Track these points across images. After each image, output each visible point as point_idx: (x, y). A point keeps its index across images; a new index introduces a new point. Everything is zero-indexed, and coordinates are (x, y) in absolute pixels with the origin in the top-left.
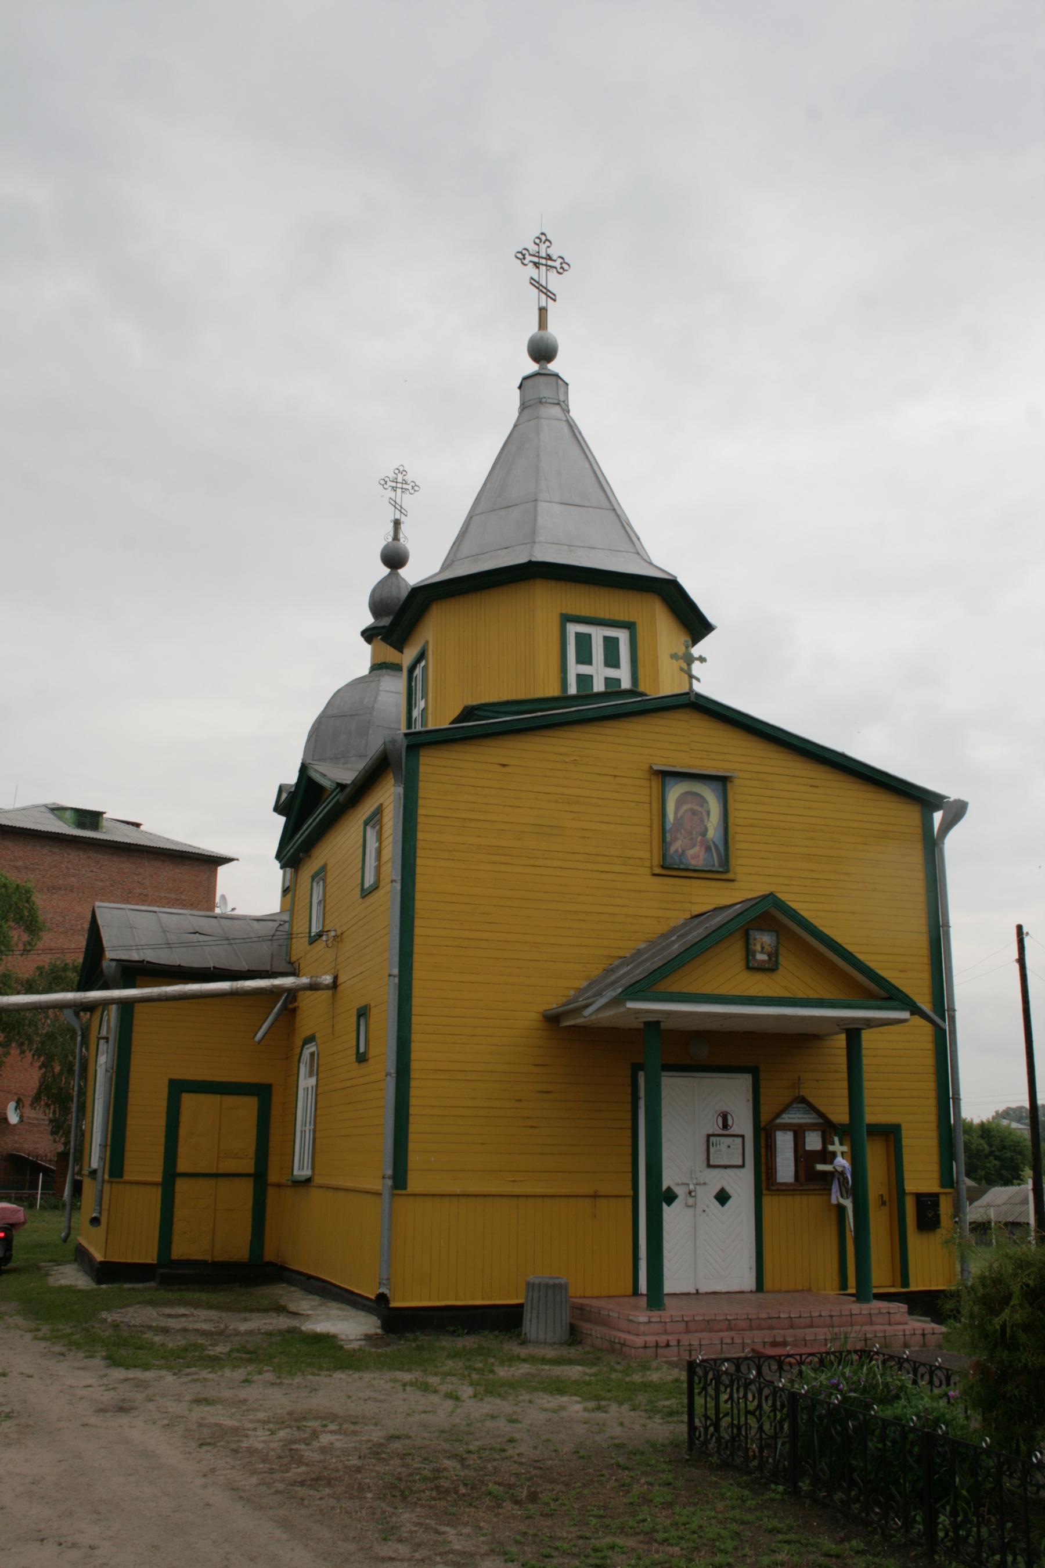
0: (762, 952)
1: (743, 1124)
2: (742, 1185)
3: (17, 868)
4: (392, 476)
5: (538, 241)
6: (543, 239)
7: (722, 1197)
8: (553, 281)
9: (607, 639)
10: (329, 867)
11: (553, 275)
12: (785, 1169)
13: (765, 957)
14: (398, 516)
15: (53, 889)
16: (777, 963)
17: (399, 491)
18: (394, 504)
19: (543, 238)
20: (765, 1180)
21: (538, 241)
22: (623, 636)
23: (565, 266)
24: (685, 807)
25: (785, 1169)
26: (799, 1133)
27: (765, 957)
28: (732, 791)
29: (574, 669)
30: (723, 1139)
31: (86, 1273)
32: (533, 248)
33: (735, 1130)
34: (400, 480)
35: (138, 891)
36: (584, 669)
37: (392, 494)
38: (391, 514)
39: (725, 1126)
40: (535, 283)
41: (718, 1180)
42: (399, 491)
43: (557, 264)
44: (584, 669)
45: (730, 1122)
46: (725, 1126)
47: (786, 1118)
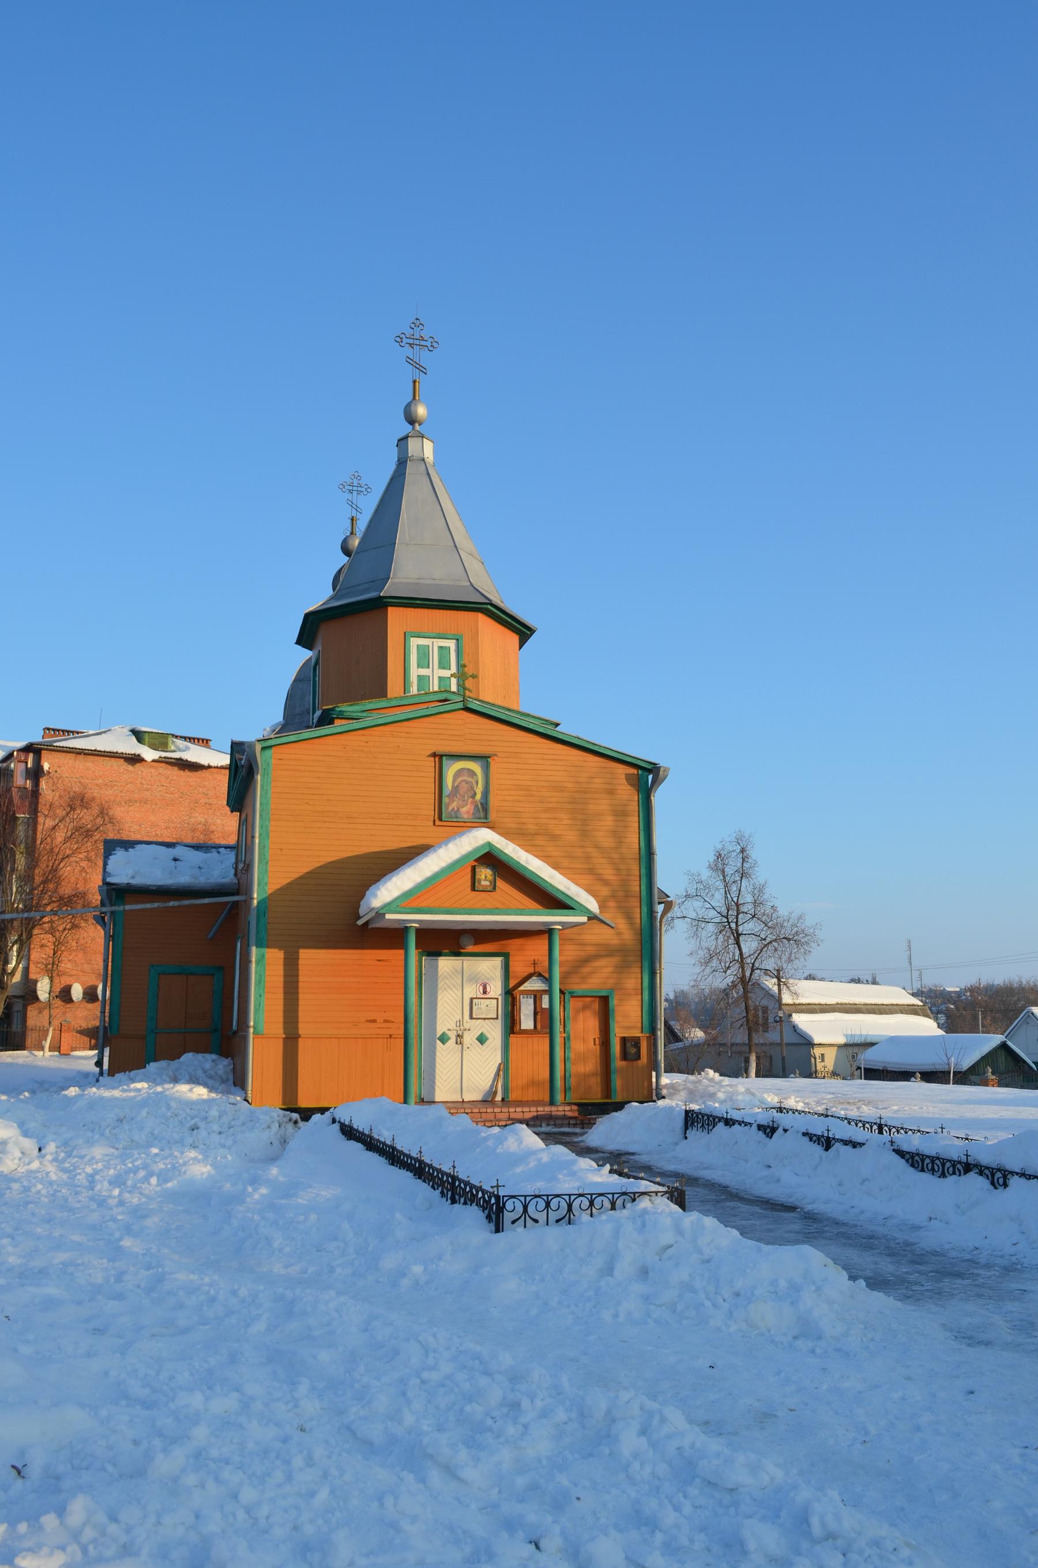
0: (485, 880)
1: (496, 989)
2: (495, 1032)
3: (97, 785)
4: (349, 481)
5: (413, 326)
6: (417, 323)
7: (482, 1039)
8: (425, 358)
9: (441, 648)
10: (429, 753)
11: (425, 353)
12: (527, 1022)
13: (488, 883)
14: (354, 514)
15: (130, 802)
16: (494, 888)
17: (355, 493)
18: (351, 504)
19: (418, 323)
20: (511, 1025)
21: (413, 326)
22: (451, 644)
23: (435, 345)
24: (460, 779)
25: (527, 1022)
26: (537, 996)
27: (488, 883)
28: (494, 765)
29: (415, 672)
30: (483, 1001)
31: (818, 1214)
32: (409, 332)
33: (492, 994)
34: (355, 484)
35: (203, 801)
36: (424, 672)
37: (349, 496)
38: (349, 512)
39: (485, 992)
40: (409, 360)
41: (477, 1027)
42: (355, 493)
43: (429, 344)
44: (424, 672)
45: (488, 989)
46: (485, 992)
47: (527, 986)
